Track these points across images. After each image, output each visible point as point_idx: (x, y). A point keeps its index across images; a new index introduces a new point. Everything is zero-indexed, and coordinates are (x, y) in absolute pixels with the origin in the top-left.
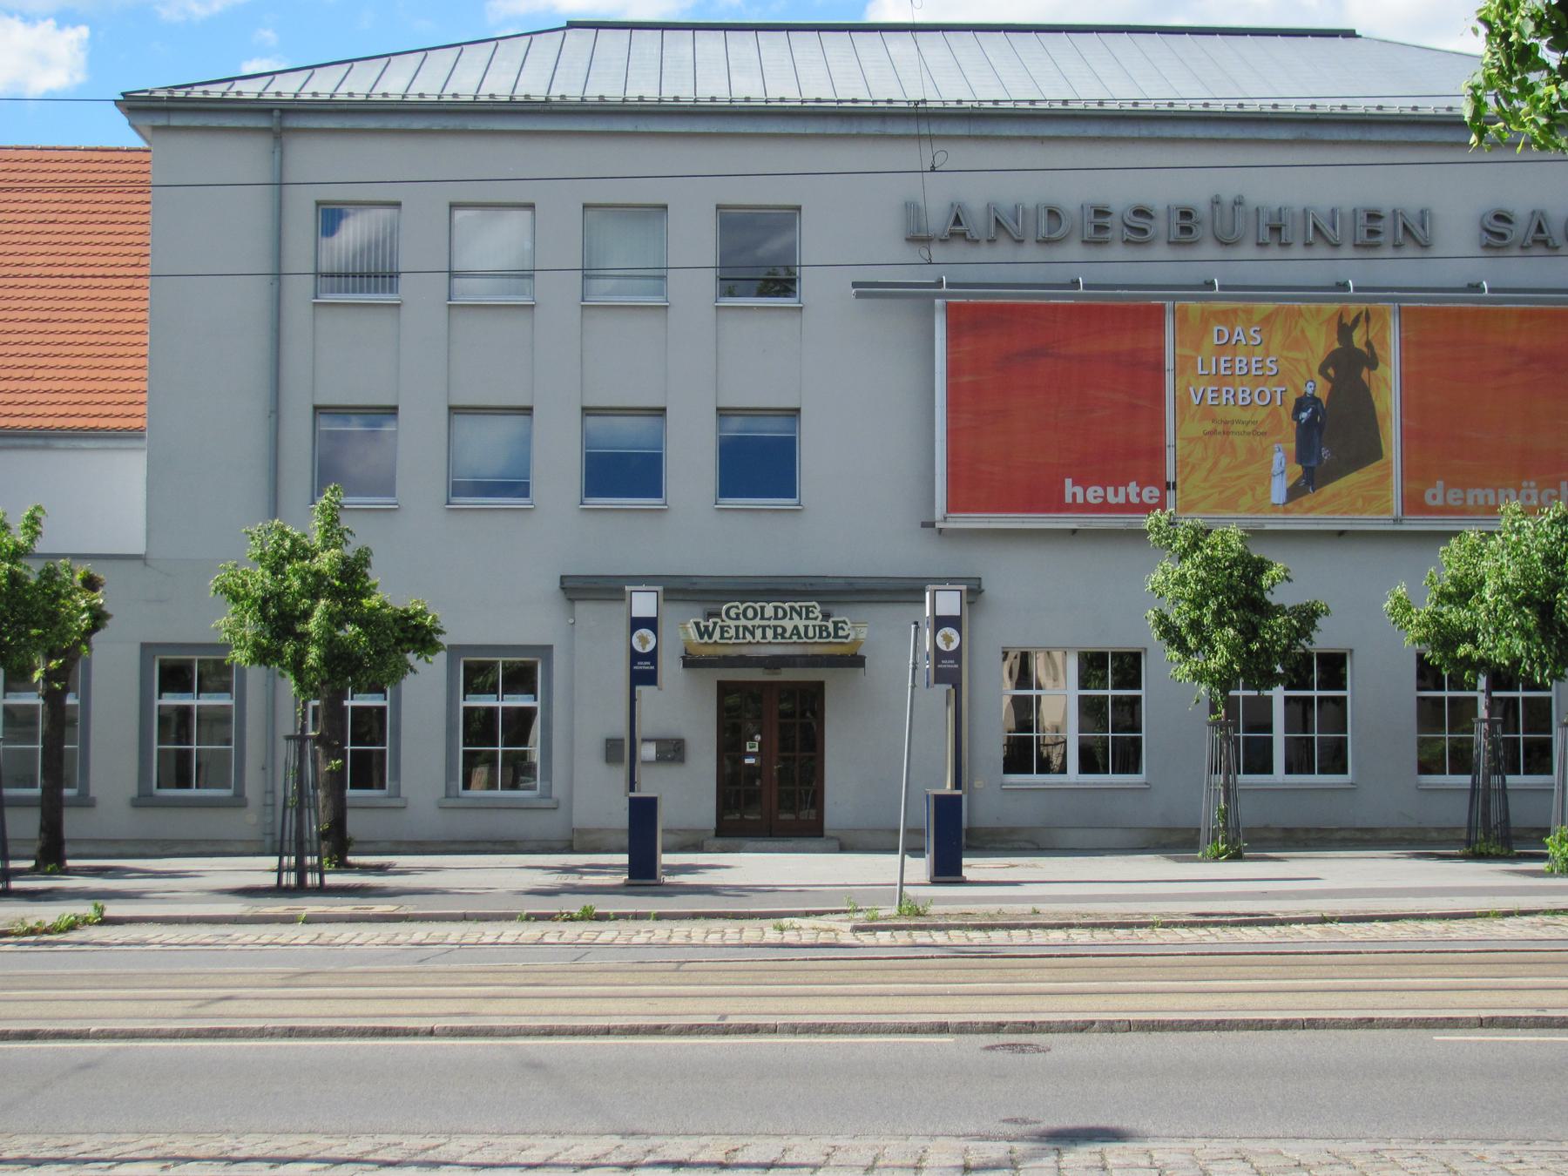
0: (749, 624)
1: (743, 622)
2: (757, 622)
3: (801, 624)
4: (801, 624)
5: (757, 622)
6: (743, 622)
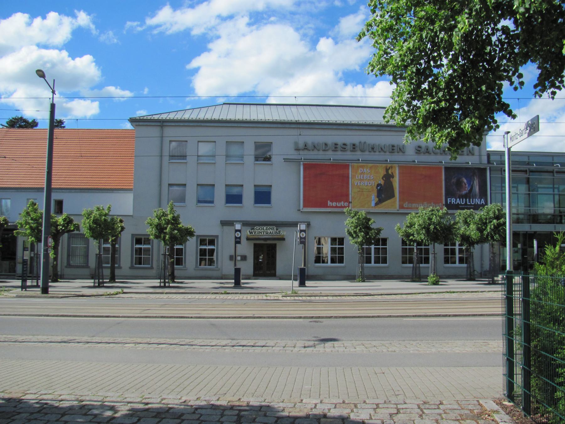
0: (261, 231)
1: (259, 231)
2: (262, 231)
3: (272, 231)
4: (272, 231)
5: (262, 231)
6: (259, 231)
